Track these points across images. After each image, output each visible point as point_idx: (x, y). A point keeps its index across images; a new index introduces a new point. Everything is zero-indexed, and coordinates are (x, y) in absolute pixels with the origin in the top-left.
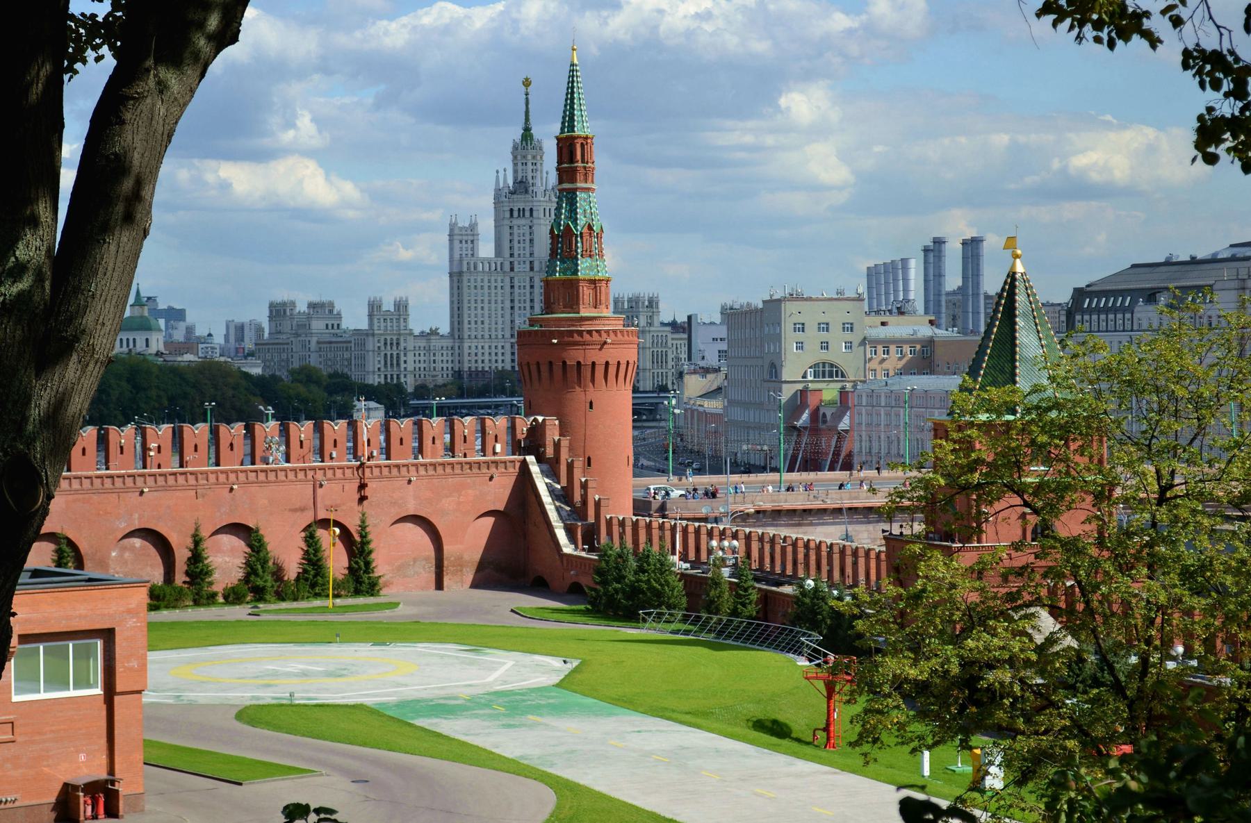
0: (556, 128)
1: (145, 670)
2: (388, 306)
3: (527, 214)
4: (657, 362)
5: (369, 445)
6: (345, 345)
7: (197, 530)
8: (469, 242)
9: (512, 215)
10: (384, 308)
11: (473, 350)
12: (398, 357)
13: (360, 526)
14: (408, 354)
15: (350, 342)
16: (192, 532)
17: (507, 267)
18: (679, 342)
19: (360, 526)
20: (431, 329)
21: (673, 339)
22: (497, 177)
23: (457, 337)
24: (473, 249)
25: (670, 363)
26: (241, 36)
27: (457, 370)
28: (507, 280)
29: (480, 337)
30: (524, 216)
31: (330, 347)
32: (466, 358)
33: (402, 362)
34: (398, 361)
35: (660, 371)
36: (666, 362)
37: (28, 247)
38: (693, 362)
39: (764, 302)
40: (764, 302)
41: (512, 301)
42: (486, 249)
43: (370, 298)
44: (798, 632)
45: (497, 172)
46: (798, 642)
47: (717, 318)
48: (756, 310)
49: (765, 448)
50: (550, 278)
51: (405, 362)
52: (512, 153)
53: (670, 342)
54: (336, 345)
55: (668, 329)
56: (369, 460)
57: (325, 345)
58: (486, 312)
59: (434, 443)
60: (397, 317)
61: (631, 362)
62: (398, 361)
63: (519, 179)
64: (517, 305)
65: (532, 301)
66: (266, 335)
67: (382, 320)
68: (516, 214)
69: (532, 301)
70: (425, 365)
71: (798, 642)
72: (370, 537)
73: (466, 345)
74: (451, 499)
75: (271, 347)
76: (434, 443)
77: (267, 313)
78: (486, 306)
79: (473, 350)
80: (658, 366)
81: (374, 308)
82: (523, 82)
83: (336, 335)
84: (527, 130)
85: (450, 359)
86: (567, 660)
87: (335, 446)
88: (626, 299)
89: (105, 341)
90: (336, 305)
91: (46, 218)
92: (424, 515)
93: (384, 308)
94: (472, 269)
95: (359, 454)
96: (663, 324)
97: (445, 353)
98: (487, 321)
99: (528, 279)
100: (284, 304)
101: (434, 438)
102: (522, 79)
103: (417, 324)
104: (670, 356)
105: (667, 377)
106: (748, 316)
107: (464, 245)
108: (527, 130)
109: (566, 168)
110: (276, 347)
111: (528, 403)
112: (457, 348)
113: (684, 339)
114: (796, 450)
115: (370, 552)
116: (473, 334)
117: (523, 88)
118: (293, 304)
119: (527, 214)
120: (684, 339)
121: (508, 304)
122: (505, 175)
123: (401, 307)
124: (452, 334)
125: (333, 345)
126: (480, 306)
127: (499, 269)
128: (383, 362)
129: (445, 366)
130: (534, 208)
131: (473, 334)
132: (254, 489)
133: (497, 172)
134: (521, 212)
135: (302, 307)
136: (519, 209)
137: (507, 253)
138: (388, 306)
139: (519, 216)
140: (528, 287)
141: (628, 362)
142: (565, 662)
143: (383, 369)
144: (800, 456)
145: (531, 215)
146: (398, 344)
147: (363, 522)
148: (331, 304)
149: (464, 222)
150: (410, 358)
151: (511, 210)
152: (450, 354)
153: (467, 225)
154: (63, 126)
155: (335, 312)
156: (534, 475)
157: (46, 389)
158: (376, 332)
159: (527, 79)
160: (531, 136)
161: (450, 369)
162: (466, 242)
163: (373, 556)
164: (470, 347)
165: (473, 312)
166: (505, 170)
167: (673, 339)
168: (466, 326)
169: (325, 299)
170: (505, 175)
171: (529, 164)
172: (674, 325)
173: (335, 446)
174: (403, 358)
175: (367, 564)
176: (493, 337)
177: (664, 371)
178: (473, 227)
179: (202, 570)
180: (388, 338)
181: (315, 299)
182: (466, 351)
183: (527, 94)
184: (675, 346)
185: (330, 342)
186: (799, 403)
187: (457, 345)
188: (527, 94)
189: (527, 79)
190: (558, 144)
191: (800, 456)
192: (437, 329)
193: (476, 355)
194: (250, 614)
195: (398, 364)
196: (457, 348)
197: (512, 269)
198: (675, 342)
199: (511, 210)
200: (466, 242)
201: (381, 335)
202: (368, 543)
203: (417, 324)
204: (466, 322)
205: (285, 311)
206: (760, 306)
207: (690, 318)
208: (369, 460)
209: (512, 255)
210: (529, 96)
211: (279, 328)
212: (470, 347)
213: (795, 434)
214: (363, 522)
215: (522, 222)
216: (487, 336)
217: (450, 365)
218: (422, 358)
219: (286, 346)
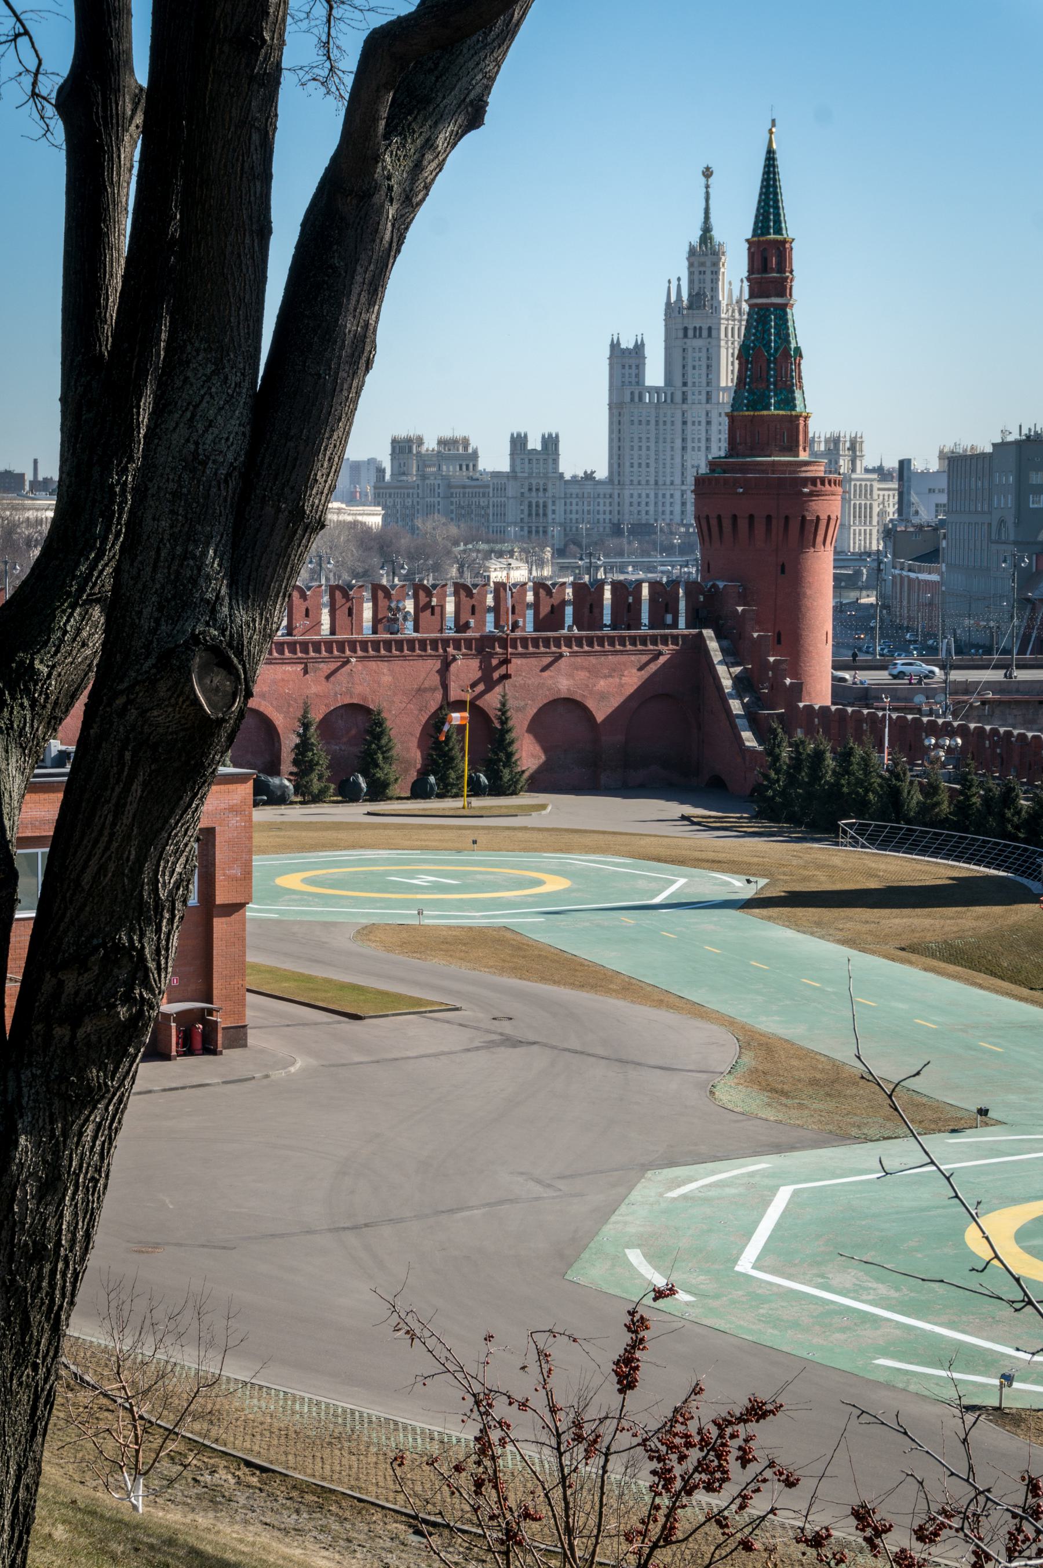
0: (747, 230)
1: (250, 879)
2: (534, 443)
3: (705, 333)
4: (865, 517)
5: (513, 613)
6: (481, 490)
7: (306, 712)
8: (634, 367)
9: (686, 336)
10: (530, 446)
11: (635, 499)
12: (545, 506)
13: (500, 710)
14: (557, 502)
15: (488, 486)
16: (299, 714)
17: (678, 397)
18: (886, 493)
19: (500, 710)
20: (585, 473)
21: (879, 489)
22: (669, 288)
23: (616, 482)
24: (637, 375)
25: (875, 521)
26: (487, 118)
27: (616, 522)
28: (679, 414)
29: (643, 482)
30: (700, 336)
31: (464, 494)
32: (627, 508)
33: (549, 513)
34: (544, 510)
35: (863, 528)
36: (871, 517)
37: (226, 383)
38: (904, 517)
39: (994, 445)
40: (994, 445)
41: (684, 440)
42: (654, 375)
43: (512, 435)
44: (1034, 852)
45: (669, 282)
46: (1032, 863)
47: (934, 466)
48: (983, 455)
49: (992, 624)
50: (735, 413)
51: (554, 512)
52: (688, 259)
53: (876, 492)
54: (470, 490)
55: (875, 476)
56: (513, 631)
57: (458, 490)
58: (652, 453)
59: (591, 612)
60: (545, 457)
61: (833, 517)
62: (544, 510)
63: (696, 290)
64: (689, 445)
65: (708, 440)
66: (388, 477)
67: (527, 461)
68: (690, 333)
69: (708, 440)
70: (578, 516)
71: (1032, 863)
72: (510, 723)
73: (627, 493)
74: (611, 680)
75: (392, 491)
76: (591, 612)
77: (389, 450)
78: (652, 445)
79: (635, 499)
80: (860, 521)
81: (518, 442)
82: (703, 173)
83: (472, 479)
84: (707, 229)
85: (608, 509)
86: (752, 879)
87: (473, 613)
88: (822, 439)
89: (317, 501)
90: (471, 442)
91: (249, 346)
92: (579, 699)
93: (530, 446)
94: (636, 399)
95: (502, 623)
96: (867, 471)
97: (601, 501)
98: (652, 465)
99: (704, 413)
100: (409, 441)
101: (591, 606)
102: (702, 168)
103: (570, 465)
104: (876, 510)
105: (871, 534)
106: (974, 461)
107: (627, 371)
108: (707, 229)
109: (774, 277)
110: (399, 491)
111: (706, 566)
112: (616, 496)
113: (894, 490)
114: (1029, 628)
115: (512, 742)
116: (635, 480)
117: (703, 180)
118: (420, 441)
119: (705, 333)
120: (894, 490)
121: (678, 443)
122: (679, 286)
123: (551, 443)
124: (610, 480)
125: (467, 490)
126: (644, 444)
127: (669, 400)
128: (526, 512)
129: (601, 517)
130: (713, 327)
131: (635, 480)
132: (373, 665)
133: (669, 282)
134: (698, 332)
135: (430, 444)
136: (695, 328)
137: (678, 382)
138: (534, 443)
139: (695, 336)
140: (704, 423)
141: (829, 517)
142: (749, 881)
143: (526, 520)
144: (1034, 635)
145: (710, 335)
146: (545, 490)
147: (503, 704)
148: (466, 442)
149: (627, 343)
150: (560, 507)
151: (686, 329)
152: (607, 504)
153: (631, 346)
154: (270, 232)
155: (470, 450)
156: (712, 653)
157: (245, 562)
158: (519, 475)
159: (708, 168)
160: (711, 238)
161: (607, 521)
162: (630, 367)
163: (514, 747)
164: (632, 496)
165: (636, 453)
166: (679, 279)
167: (879, 489)
168: (627, 469)
169: (459, 434)
170: (679, 286)
171: (708, 273)
172: (881, 472)
173: (473, 613)
174: (550, 507)
175: (510, 755)
176: (660, 482)
177: (868, 528)
178: (639, 349)
179: (312, 760)
180: (534, 482)
181: (447, 434)
182: (627, 501)
183: (707, 187)
184: (881, 498)
185: (464, 487)
186: (1034, 570)
187: (616, 492)
188: (707, 187)
189: (708, 168)
190: (749, 249)
191: (1034, 635)
192: (593, 473)
193: (639, 504)
194: (369, 814)
195: (545, 515)
196: (616, 496)
197: (684, 400)
198: (882, 493)
199: (686, 329)
200: (630, 367)
201: (526, 478)
202: (509, 731)
203: (570, 465)
204: (628, 464)
205: (410, 448)
206: (989, 449)
207: (902, 463)
208: (513, 631)
209: (685, 384)
210: (710, 190)
211: (402, 470)
212: (632, 496)
213: (1029, 606)
214: (503, 704)
215: (698, 343)
216: (652, 482)
217: (608, 517)
218: (574, 508)
219: (411, 491)
